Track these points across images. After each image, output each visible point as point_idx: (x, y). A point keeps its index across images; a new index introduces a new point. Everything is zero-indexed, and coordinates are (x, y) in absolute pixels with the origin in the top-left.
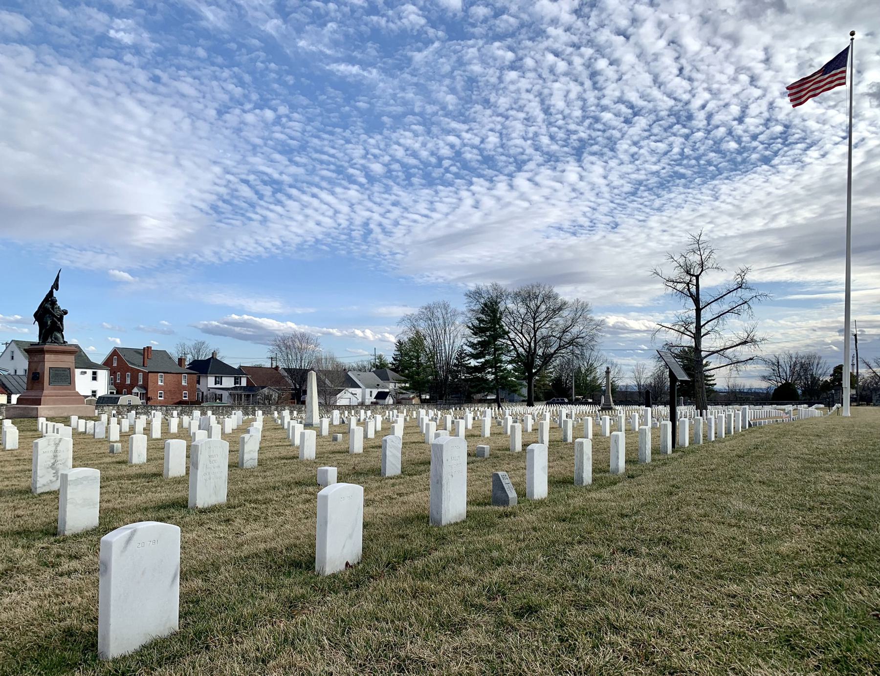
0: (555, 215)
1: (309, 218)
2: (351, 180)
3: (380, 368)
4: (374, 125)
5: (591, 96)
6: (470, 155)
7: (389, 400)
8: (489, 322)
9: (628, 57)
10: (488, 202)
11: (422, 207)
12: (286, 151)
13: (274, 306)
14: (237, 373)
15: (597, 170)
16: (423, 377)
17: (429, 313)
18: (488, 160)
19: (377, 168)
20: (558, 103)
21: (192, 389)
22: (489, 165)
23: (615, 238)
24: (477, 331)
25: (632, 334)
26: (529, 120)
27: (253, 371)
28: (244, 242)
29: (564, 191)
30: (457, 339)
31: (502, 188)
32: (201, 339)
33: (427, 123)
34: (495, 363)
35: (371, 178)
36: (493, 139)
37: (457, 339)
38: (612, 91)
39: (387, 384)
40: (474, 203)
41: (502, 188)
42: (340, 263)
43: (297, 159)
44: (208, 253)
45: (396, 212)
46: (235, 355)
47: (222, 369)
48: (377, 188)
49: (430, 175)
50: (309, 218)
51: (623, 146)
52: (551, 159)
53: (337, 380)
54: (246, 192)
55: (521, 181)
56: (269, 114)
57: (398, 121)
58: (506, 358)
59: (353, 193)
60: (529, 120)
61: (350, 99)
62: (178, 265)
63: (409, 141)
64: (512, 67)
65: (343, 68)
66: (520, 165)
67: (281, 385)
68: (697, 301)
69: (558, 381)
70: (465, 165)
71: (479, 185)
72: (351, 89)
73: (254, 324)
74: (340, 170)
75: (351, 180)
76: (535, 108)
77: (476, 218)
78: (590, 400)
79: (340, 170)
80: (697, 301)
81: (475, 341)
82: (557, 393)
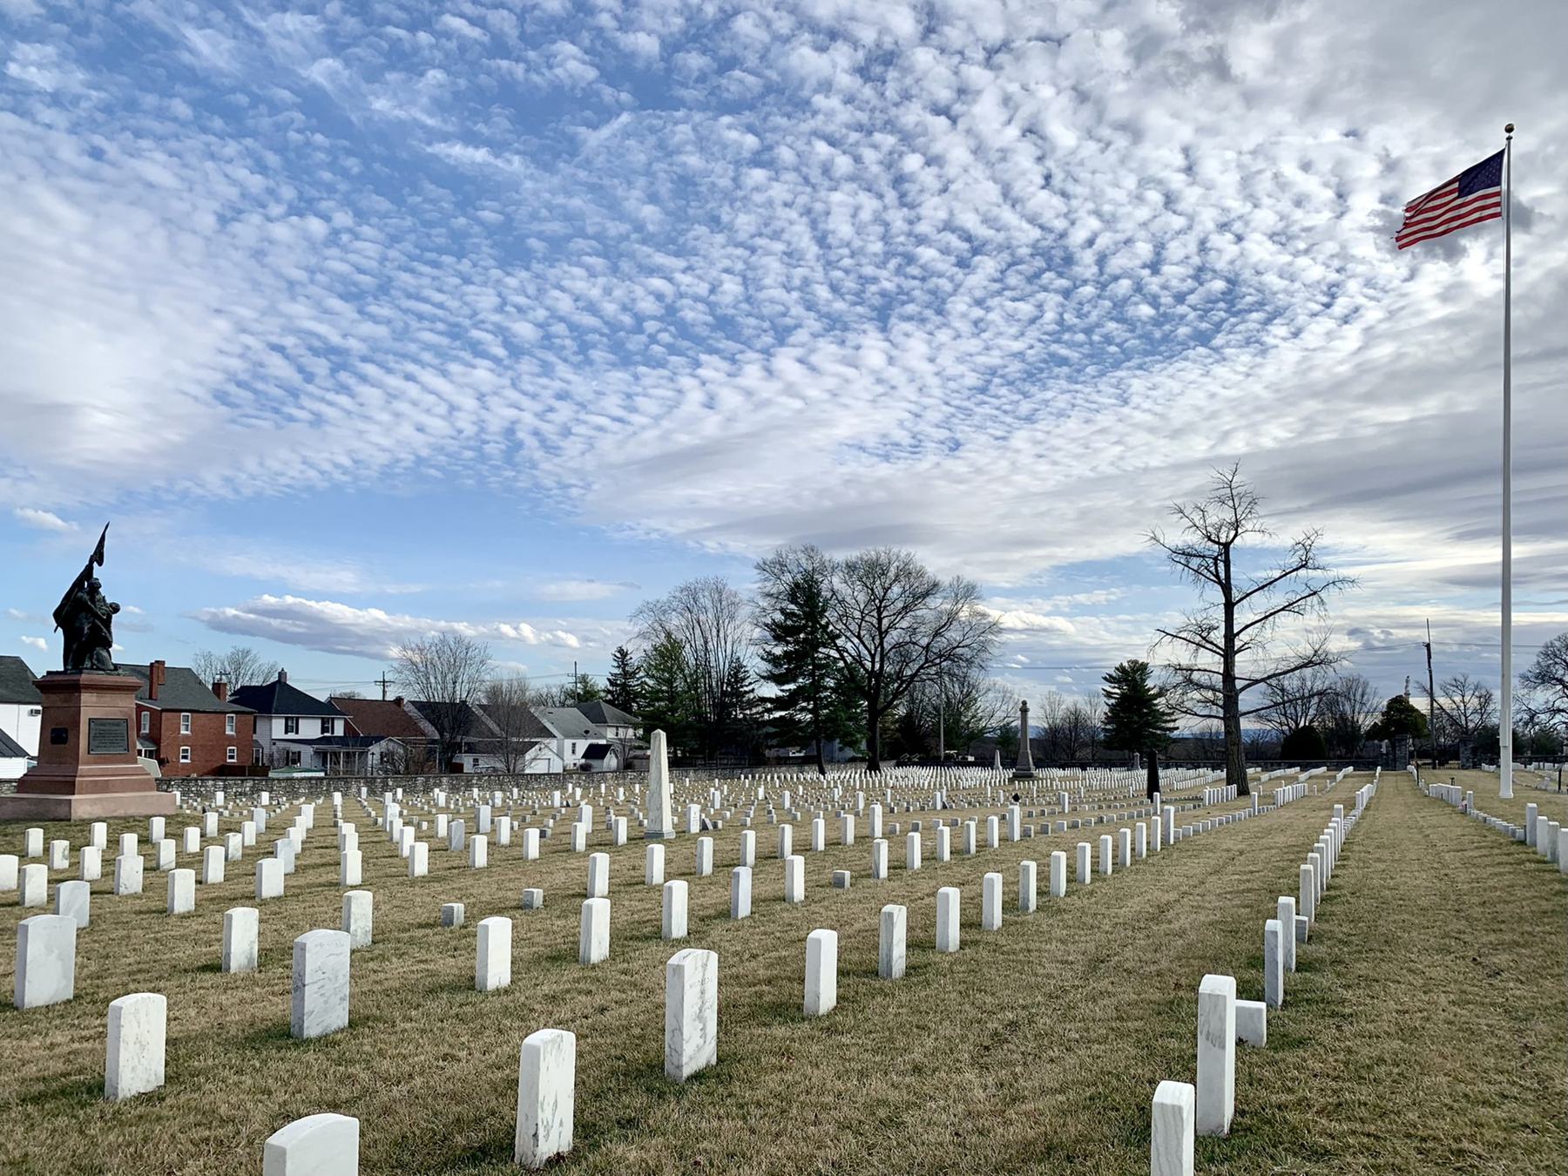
0: (889, 419)
2: (478, 350)
3: (583, 698)
4: (513, 253)
5: (897, 218)
6: (692, 314)
7: (611, 761)
8: (803, 616)
9: (958, 152)
10: (730, 399)
11: (612, 404)
12: (354, 295)
13: (346, 578)
14: (325, 710)
15: (916, 346)
17: (690, 599)
18: (725, 324)
19: (525, 331)
20: (842, 227)
21: (246, 740)
22: (729, 332)
23: (957, 466)
24: (780, 632)
25: (1046, 643)
26: (792, 256)
28: (285, 460)
29: (862, 383)
30: (746, 648)
31: (752, 373)
33: (612, 253)
35: (515, 350)
36: (732, 287)
37: (746, 648)
38: (933, 210)
39: (601, 730)
40: (709, 399)
41: (752, 373)
42: (475, 498)
45: (565, 411)
46: (316, 677)
48: (526, 365)
49: (622, 345)
51: (959, 305)
52: (835, 325)
54: (278, 367)
55: (785, 361)
56: (316, 226)
57: (558, 248)
59: (483, 374)
60: (792, 256)
63: (579, 285)
64: (757, 161)
66: (782, 335)
67: (445, 734)
68: (1227, 588)
70: (684, 330)
71: (713, 369)
72: (468, 189)
74: (455, 332)
75: (478, 350)
77: (711, 425)
78: (971, 759)
79: (455, 332)
80: (1227, 588)
81: (778, 651)
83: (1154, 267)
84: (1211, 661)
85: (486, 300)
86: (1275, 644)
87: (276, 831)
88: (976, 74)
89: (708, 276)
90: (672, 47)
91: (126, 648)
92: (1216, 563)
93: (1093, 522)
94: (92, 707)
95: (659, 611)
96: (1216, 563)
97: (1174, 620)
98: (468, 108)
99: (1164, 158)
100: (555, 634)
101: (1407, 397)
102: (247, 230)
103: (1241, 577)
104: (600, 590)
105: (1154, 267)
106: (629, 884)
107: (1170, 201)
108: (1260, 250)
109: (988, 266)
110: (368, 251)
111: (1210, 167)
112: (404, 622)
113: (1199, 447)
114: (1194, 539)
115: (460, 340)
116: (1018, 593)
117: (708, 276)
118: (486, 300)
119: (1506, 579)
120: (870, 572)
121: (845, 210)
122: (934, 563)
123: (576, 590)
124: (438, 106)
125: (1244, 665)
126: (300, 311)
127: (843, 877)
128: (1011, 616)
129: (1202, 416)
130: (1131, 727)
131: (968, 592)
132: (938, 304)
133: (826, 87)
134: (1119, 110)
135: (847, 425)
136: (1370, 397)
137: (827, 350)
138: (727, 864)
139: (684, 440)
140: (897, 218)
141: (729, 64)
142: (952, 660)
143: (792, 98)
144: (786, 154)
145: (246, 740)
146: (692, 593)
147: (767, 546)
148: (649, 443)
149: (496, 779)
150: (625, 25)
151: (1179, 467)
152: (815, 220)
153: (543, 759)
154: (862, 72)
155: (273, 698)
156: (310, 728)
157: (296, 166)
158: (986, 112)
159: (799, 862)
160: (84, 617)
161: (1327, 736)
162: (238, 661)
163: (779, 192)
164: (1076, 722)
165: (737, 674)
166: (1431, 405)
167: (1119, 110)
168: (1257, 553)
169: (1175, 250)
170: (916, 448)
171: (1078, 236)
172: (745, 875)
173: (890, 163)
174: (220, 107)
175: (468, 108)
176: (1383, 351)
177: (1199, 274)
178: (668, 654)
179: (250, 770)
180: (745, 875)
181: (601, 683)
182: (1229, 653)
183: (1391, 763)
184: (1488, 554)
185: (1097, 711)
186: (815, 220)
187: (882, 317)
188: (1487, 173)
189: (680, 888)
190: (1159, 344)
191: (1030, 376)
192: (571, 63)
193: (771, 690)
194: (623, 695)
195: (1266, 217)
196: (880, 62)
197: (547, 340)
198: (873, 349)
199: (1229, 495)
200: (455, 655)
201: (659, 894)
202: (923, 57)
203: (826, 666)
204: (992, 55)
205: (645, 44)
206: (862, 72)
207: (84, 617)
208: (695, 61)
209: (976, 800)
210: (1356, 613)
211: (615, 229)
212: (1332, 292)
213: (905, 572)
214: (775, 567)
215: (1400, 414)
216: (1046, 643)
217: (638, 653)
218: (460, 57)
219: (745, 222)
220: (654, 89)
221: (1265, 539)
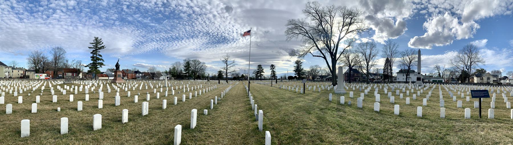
0: (194, 47)
1: (151, 46)
2: (154, 41)
3: (166, 73)
4: (156, 32)
5: (193, 29)
6: (174, 37)
8: (188, 65)
9: (198, 23)
10: (178, 45)
11: (167, 45)
12: (143, 37)
13: (144, 61)
14: (142, 73)
15: (196, 40)
16: (175, 75)
17: (176, 63)
18: (177, 38)
19: (158, 39)
20: (187, 29)
21: (135, 76)
22: (177, 39)
23: (201, 51)
24: (185, 67)
25: (212, 68)
26: (183, 32)
27: (144, 73)
28: (138, 52)
29: (191, 43)
30: (182, 68)
31: (180, 43)
32: (314, 64)
33: (166, 32)
34: (188, 73)
35: (157, 41)
36: (177, 35)
37: (182, 68)
38: (196, 28)
40: (177, 45)
41: (180, 43)
42: (157, 54)
43: (295, 31)
44: (132, 54)
45: (162, 46)
46: (141, 70)
47: (140, 73)
48: (159, 42)
49: (167, 40)
50: (151, 46)
51: (199, 37)
52: (188, 38)
53: (159, 75)
54: (137, 44)
55: (183, 41)
56: (139, 31)
57: (160, 32)
58: (191, 72)
59: (154, 43)
60: (183, 32)
61: (152, 28)
62: (128, 56)
63: (163, 35)
64: (179, 23)
65: (152, 24)
66: (183, 39)
67: (152, 76)
69: (198, 76)
70: (173, 38)
71: (176, 42)
72: (152, 27)
73: (145, 65)
74: (152, 40)
75: (154, 41)
76: (184, 30)
77: (177, 47)
79: (152, 40)
82: (199, 78)
83: (217, 35)
84: (225, 71)
85: (154, 36)
86: (231, 69)
87: (134, 85)
88: (199, 17)
89: (175, 34)
90: (170, 14)
91: (121, 69)
92: (226, 62)
93: (216, 58)
94: (118, 73)
95: (173, 64)
96: (226, 62)
97: (222, 67)
98: (151, 20)
99: (217, 26)
100: (163, 66)
101: (240, 49)
102: (133, 32)
103: (228, 63)
104: (167, 62)
105: (217, 35)
106: (170, 90)
107: (218, 29)
108: (227, 35)
109: (202, 34)
110: (144, 33)
111: (221, 27)
112: (150, 65)
113: (224, 52)
114: (224, 59)
115: (152, 40)
116: (208, 64)
117: (175, 34)
118: (154, 36)
119: (249, 65)
120: (195, 61)
121: (188, 28)
122: (201, 60)
123: (165, 62)
124: (150, 20)
125: (228, 71)
126: (138, 39)
127: (179, 92)
128: (208, 66)
129: (223, 50)
130: (220, 77)
131: (204, 63)
132: (197, 37)
133: (185, 17)
134: (212, 21)
135: (189, 48)
136: (237, 49)
137: (187, 40)
138: (164, 91)
139: (174, 48)
140: (193, 29)
141: (175, 15)
142: (203, 69)
143: (181, 18)
144: (181, 23)
145: (135, 76)
146: (177, 63)
147: (184, 58)
148: (171, 49)
149: (156, 80)
150: (165, 12)
151: (222, 53)
152: (185, 29)
153: (161, 78)
154: (188, 16)
155: (137, 72)
156: (141, 75)
157: (137, 27)
158: (200, 20)
159: (174, 91)
160: (117, 66)
161: (237, 78)
162: (135, 69)
163: (181, 26)
164: (215, 76)
165: (181, 71)
166: (242, 50)
167: (212, 21)
168: (230, 61)
169: (219, 34)
170: (197, 50)
171: (210, 32)
172: (167, 92)
173: (192, 24)
174: (130, 23)
175: (151, 20)
176: (238, 45)
177: (222, 36)
178: (174, 68)
179: (135, 78)
180: (167, 92)
181: (168, 71)
182: (227, 70)
183: (241, 80)
184: (248, 63)
185: (217, 75)
186: (185, 29)
187: (192, 37)
188: (249, 31)
189: (158, 93)
190: (219, 42)
191: (207, 44)
192: (160, 15)
193: (184, 72)
194: (170, 72)
195: (227, 32)
196: (189, 15)
197: (160, 40)
198: (192, 40)
199: (227, 56)
200: (154, 68)
201: (172, 91)
202: (193, 15)
203: (190, 70)
204: (200, 15)
205: (167, 14)
206: (188, 16)
207: (117, 66)
208: (172, 15)
209: (215, 84)
210: (238, 67)
211: (166, 29)
212: (233, 39)
213: (198, 61)
214: (185, 60)
215: (240, 50)
216: (212, 68)
217: (172, 68)
218: (150, 16)
219: (178, 29)
220: (168, 18)
221: (231, 60)
